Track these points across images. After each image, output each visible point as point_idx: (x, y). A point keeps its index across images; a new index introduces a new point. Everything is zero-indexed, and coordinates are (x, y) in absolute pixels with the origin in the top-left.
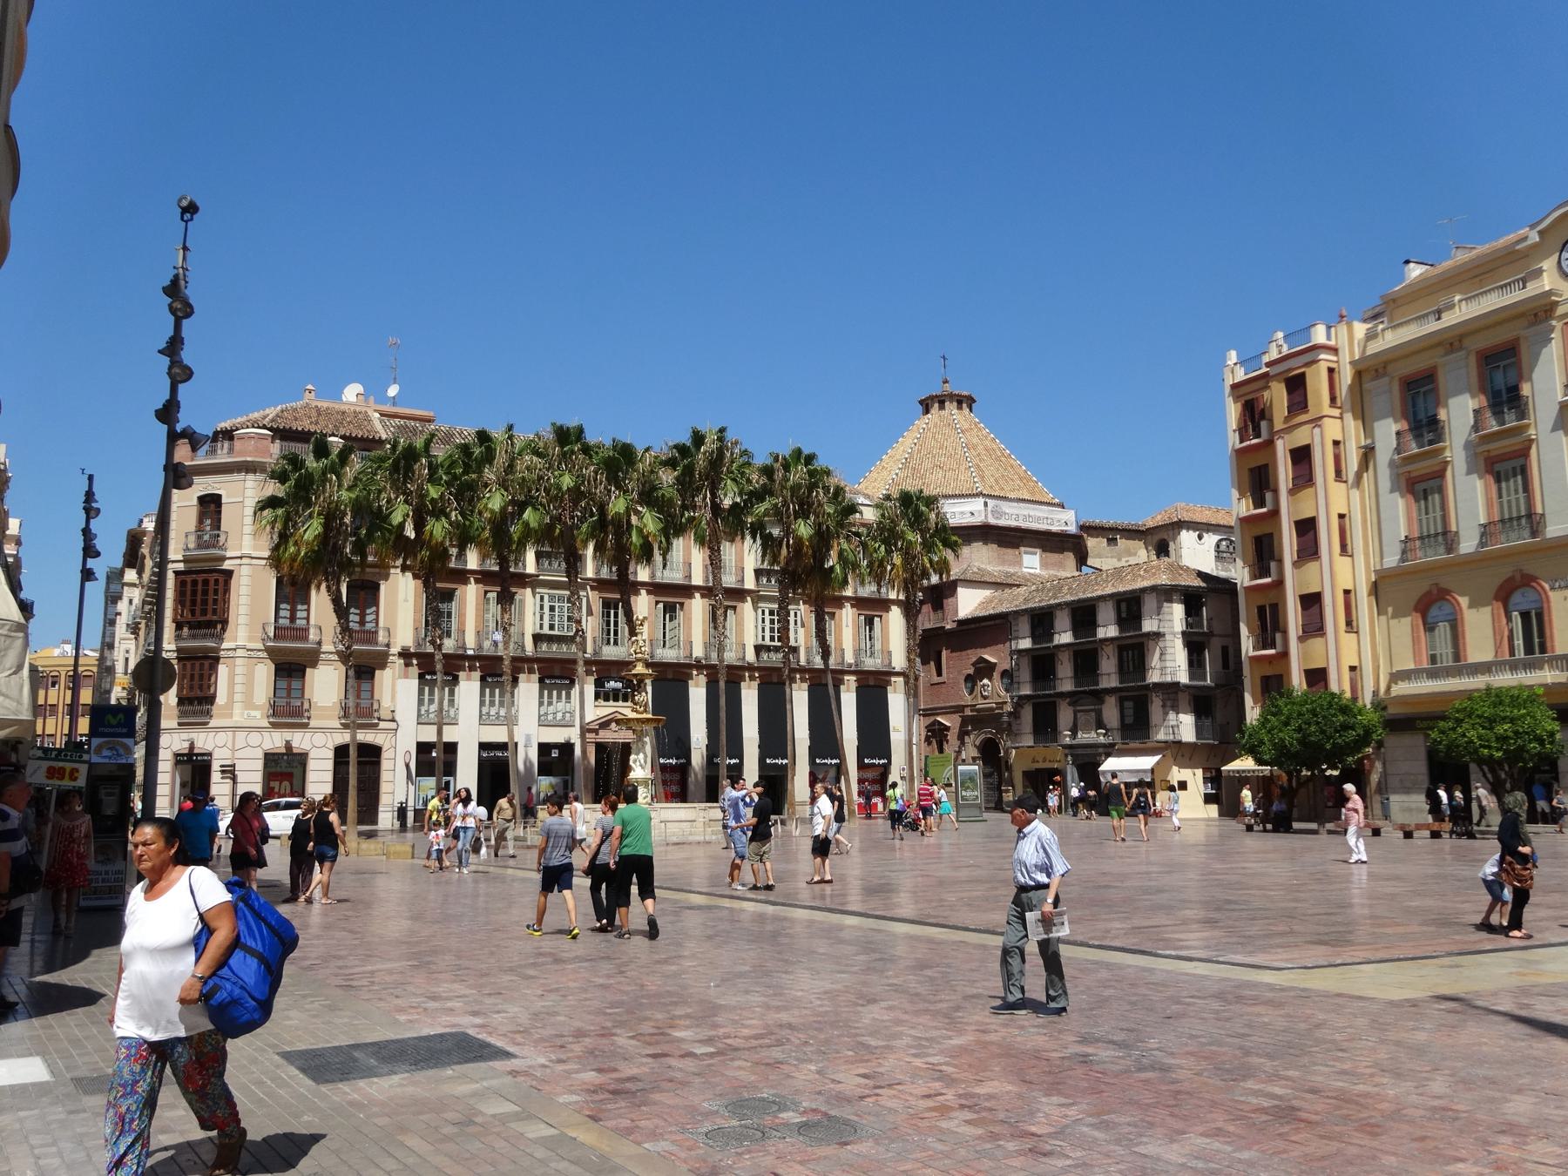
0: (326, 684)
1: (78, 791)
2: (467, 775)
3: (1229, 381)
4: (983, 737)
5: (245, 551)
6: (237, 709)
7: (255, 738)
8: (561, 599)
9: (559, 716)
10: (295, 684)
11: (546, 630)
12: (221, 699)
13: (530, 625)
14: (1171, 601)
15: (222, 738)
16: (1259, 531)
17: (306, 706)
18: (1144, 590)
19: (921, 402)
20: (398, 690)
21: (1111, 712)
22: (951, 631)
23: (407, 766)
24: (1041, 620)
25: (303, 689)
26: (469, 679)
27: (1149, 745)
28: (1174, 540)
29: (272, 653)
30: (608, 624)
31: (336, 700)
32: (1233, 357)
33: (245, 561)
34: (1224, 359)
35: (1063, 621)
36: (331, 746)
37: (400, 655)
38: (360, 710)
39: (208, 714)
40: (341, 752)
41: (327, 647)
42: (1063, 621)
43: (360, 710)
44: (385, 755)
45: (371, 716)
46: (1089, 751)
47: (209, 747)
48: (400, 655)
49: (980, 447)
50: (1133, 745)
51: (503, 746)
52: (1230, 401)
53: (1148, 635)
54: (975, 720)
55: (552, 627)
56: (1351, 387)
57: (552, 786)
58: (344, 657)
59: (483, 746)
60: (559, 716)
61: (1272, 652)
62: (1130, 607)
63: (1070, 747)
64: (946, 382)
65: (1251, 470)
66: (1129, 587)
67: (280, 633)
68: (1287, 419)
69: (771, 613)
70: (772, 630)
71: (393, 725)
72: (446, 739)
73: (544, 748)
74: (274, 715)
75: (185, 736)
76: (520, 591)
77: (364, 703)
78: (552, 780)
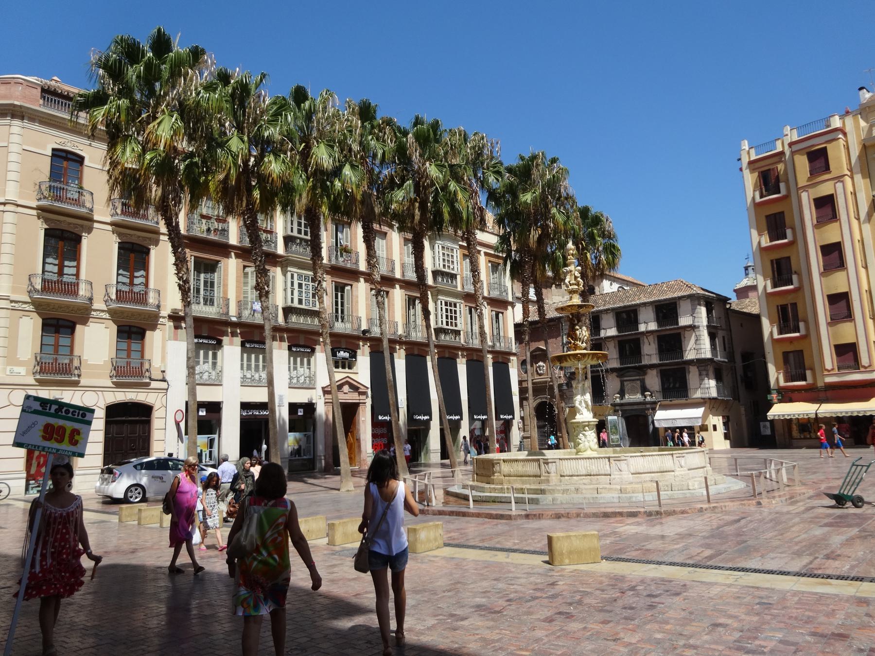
0: (96, 342)
1: (805, 188)
4: (539, 401)
5: (10, 196)
8: (306, 278)
9: (302, 379)
10: (64, 341)
11: (296, 304)
13: (279, 298)
14: (700, 305)
16: (776, 255)
17: (76, 363)
18: (680, 298)
20: (167, 350)
21: (653, 380)
23: (178, 424)
25: (72, 347)
26: (231, 344)
27: (689, 401)
28: (599, 285)
29: (39, 307)
30: (337, 304)
32: (745, 145)
33: (8, 207)
34: (740, 145)
37: (171, 317)
38: (130, 370)
41: (99, 304)
43: (130, 370)
44: (156, 414)
45: (141, 375)
46: (640, 407)
48: (171, 317)
51: (262, 406)
53: (685, 328)
55: (300, 302)
56: (859, 157)
57: (298, 441)
58: (115, 315)
59: (245, 406)
60: (302, 379)
61: (797, 334)
63: (621, 405)
65: (767, 217)
67: (47, 286)
68: (809, 179)
71: (163, 385)
73: (293, 407)
74: (41, 372)
76: (272, 269)
77: (135, 363)
78: (297, 434)
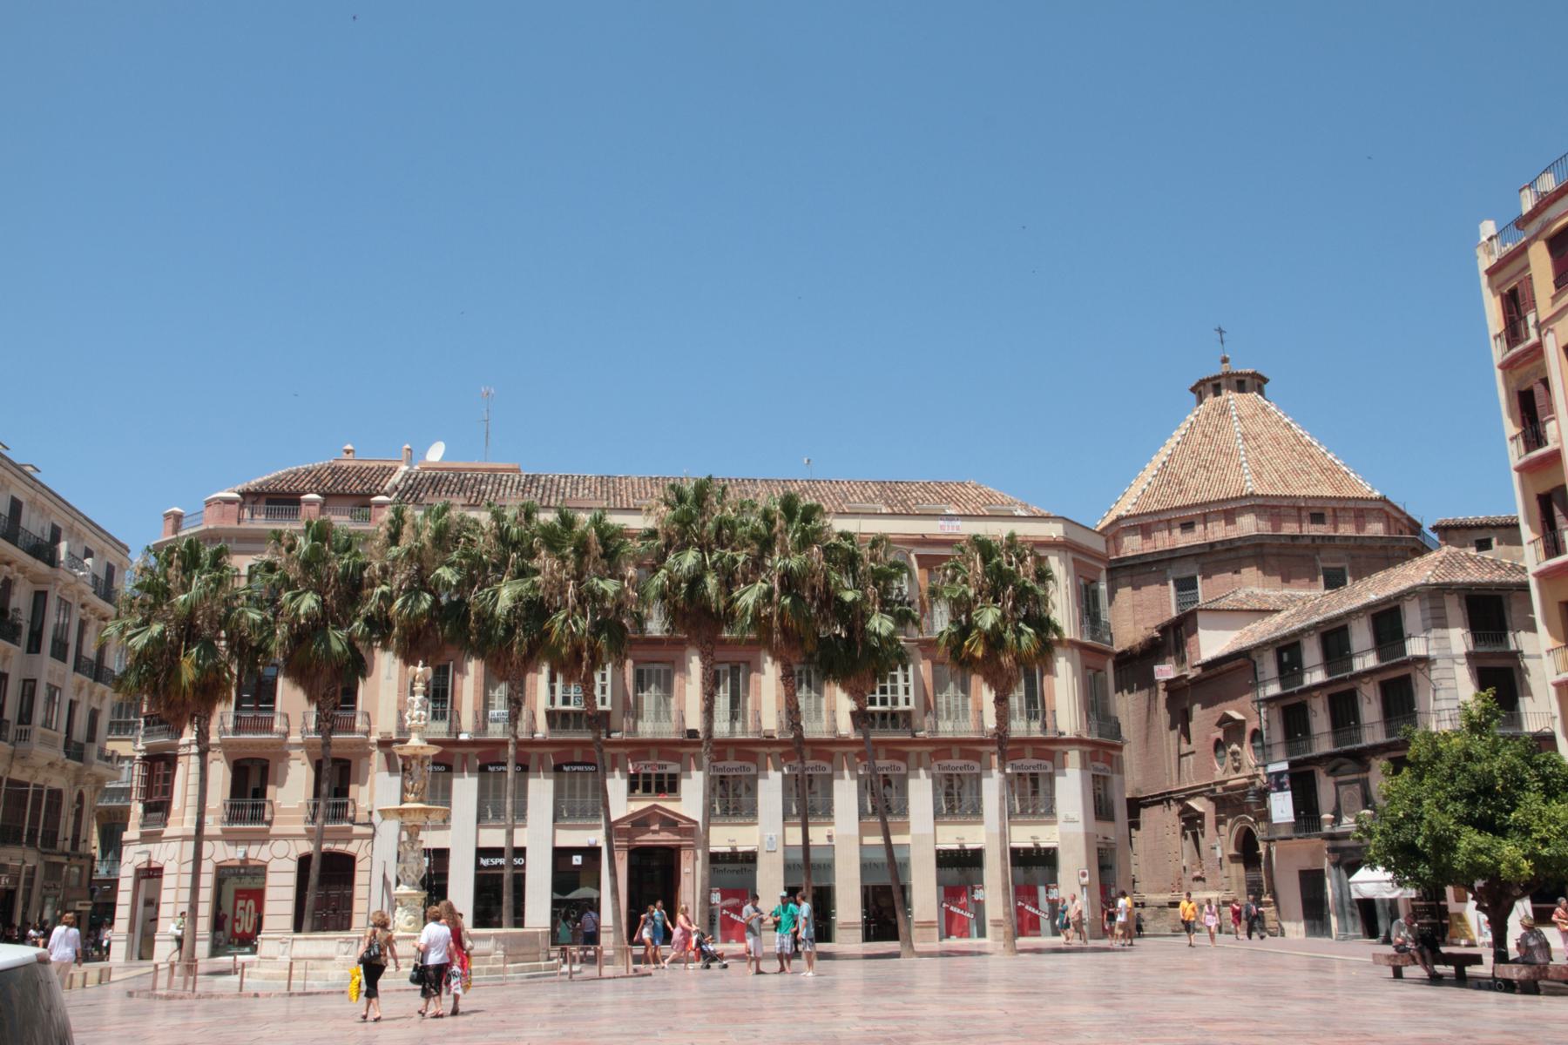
2: (461, 891)
3: (1485, 262)
18: (1401, 596)
19: (1193, 390)
22: (1196, 682)
24: (1287, 651)
35: (1312, 653)
36: (294, 855)
40: (304, 862)
42: (1312, 653)
44: (359, 866)
52: (1487, 293)
54: (1230, 802)
59: (482, 852)
62: (1387, 622)
64: (1225, 360)
66: (1382, 595)
68: (1555, 298)
71: (369, 831)
72: (517, 844)
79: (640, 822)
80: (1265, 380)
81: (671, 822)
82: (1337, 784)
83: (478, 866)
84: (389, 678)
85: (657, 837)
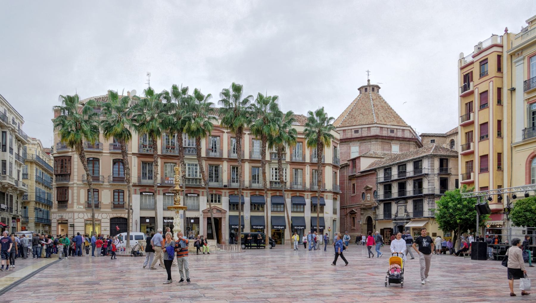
2: (203, 229)
6: (75, 205)
7: (81, 215)
12: (70, 202)
15: (70, 215)
18: (423, 157)
19: (359, 89)
31: (110, 202)
36: (109, 218)
39: (66, 206)
47: (67, 218)
49: (379, 106)
50: (417, 219)
69: (276, 169)
70: (276, 176)
75: (60, 215)
79: (210, 210)
80: (380, 88)
81: (220, 211)
82: (398, 206)
83: (164, 222)
84: (135, 166)
85: (216, 215)
